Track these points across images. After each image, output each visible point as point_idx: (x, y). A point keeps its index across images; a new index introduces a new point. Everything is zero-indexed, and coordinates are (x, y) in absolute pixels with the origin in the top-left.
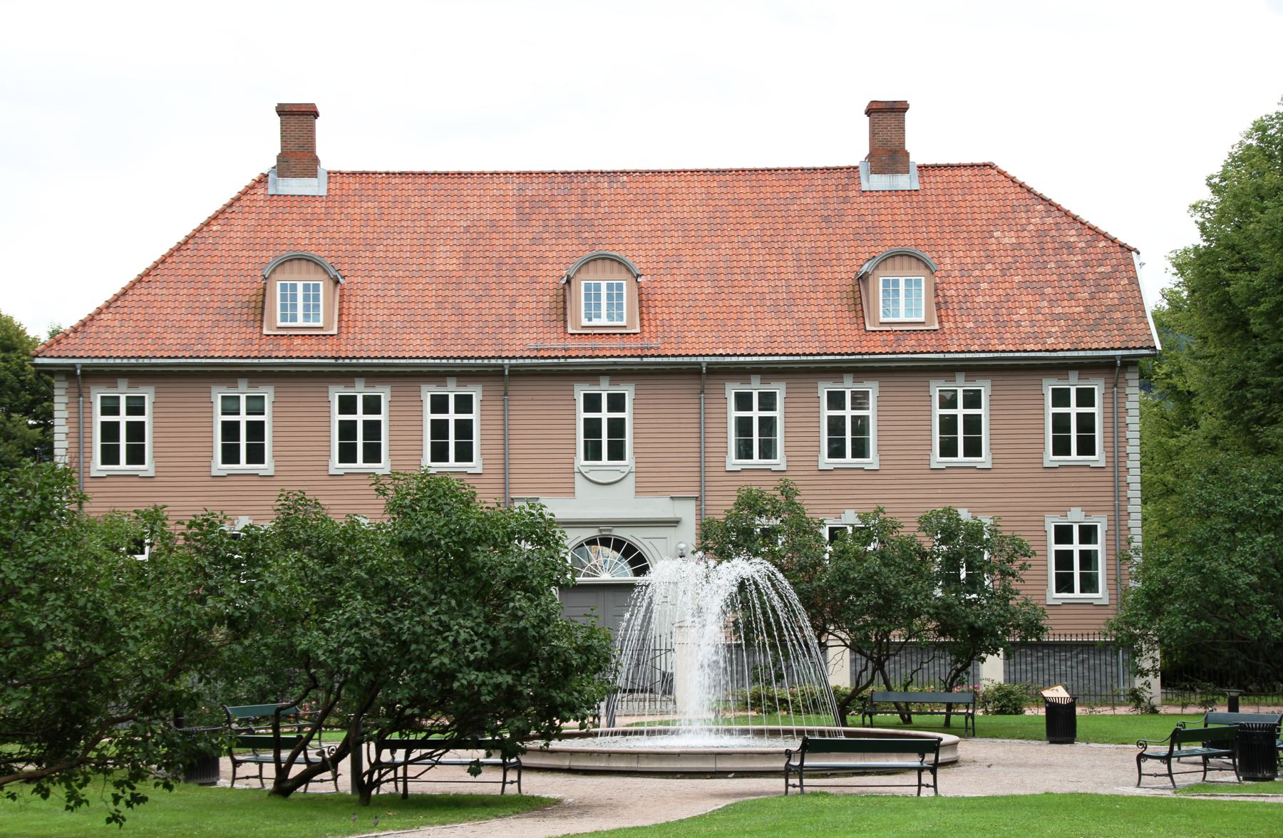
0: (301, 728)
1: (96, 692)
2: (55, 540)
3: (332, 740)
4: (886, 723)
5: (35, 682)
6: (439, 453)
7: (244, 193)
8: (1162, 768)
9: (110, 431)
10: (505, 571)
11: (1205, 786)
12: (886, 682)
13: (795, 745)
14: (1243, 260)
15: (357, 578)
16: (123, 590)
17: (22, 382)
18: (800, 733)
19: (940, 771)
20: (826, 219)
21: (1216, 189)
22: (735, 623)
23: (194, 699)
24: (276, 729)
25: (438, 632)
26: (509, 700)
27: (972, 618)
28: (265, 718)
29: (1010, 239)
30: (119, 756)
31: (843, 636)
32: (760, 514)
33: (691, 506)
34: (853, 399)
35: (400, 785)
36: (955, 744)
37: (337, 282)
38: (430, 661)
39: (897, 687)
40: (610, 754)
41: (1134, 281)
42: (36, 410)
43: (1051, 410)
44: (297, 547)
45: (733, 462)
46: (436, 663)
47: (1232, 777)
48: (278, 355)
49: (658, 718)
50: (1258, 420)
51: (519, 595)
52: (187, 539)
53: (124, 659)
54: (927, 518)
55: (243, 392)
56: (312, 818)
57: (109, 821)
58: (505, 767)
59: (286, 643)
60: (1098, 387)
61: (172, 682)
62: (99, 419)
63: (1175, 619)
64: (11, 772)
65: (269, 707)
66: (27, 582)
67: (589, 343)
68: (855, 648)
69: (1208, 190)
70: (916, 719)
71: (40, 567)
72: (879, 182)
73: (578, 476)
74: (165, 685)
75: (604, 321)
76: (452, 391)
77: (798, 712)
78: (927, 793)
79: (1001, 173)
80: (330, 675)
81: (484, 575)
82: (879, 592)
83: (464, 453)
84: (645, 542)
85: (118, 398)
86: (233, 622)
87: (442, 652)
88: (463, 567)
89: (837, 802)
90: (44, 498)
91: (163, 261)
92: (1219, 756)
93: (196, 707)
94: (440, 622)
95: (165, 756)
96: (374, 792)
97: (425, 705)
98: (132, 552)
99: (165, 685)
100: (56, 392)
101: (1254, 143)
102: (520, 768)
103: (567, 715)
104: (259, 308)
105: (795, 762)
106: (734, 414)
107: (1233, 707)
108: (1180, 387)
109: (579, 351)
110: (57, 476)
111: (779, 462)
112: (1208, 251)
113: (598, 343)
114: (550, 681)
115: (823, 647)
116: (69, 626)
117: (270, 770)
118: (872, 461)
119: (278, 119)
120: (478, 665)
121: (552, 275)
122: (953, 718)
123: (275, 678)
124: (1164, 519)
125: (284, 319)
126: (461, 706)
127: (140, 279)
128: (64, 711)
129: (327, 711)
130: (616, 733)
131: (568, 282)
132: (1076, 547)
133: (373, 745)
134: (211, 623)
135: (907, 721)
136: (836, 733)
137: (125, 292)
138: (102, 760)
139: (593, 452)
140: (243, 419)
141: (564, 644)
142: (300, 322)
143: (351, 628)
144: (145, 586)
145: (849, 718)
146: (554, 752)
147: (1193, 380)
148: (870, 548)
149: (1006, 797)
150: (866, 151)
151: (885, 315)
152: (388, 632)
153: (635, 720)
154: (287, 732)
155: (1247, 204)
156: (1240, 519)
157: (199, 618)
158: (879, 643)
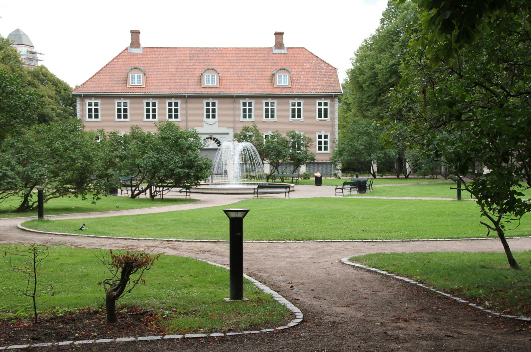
0: (137, 182)
1: (88, 173)
2: (77, 136)
3: (145, 185)
4: (278, 182)
5: (73, 170)
6: (170, 117)
7: (122, 52)
8: (341, 191)
9: (90, 110)
10: (187, 145)
11: (350, 195)
12: (278, 172)
13: (256, 187)
14: (362, 72)
15: (151, 147)
16: (94, 149)
17: (69, 98)
18: (257, 184)
19: (290, 193)
20: (264, 60)
21: (356, 55)
22: (242, 158)
23: (111, 175)
24: (131, 182)
25: (171, 160)
26: (188, 176)
27: (298, 157)
28: (129, 180)
29: (308, 66)
30: (94, 188)
31: (268, 161)
32: (248, 132)
33: (232, 130)
34: (271, 104)
35: (161, 196)
36: (294, 186)
37: (145, 74)
38: (169, 166)
39: (281, 173)
40: (212, 189)
41: (337, 76)
42: (73, 105)
43: (291, 107)
44: (136, 139)
45: (242, 119)
46: (170, 167)
47: (356, 193)
48: (130, 92)
49: (224, 181)
50: (365, 110)
51: (190, 151)
52: (110, 137)
53: (94, 165)
54: (288, 133)
55: (122, 101)
56: (140, 204)
57: (92, 203)
58: (186, 192)
59: (133, 162)
60: (328, 101)
61: (106, 171)
62: (88, 107)
63: (345, 157)
64: (69, 191)
65: (130, 177)
66: (71, 146)
67: (206, 90)
68: (271, 164)
69: (354, 55)
70: (285, 181)
71: (74, 143)
72: (277, 51)
73: (204, 122)
74: (104, 172)
75: (210, 84)
76: (173, 101)
77: (257, 179)
78: (287, 198)
79: (306, 50)
80: (144, 170)
81: (182, 146)
82: (277, 151)
83: (176, 117)
84: (221, 139)
85: (121, 103)
86: (121, 158)
87: (171, 164)
88: (176, 144)
89: (266, 200)
90: (75, 126)
91: (102, 69)
92: (354, 188)
93: (112, 177)
94: (171, 157)
95: (105, 189)
96: (155, 198)
97: (168, 177)
98: (96, 140)
99: (104, 172)
100: (77, 101)
101: (364, 44)
102: (190, 192)
103: (201, 179)
104: (126, 81)
105: (256, 191)
106: (242, 107)
107: (357, 177)
108: (347, 102)
109: (204, 92)
110: (78, 121)
111: (253, 119)
112: (354, 70)
113: (209, 90)
114: (197, 171)
115: (263, 164)
116: (81, 157)
117: (130, 192)
118: (275, 119)
119: (131, 34)
120: (180, 167)
121: (198, 73)
122: (294, 180)
123: (131, 170)
124: (343, 133)
125: (132, 83)
126: (176, 177)
127: (97, 73)
128: (81, 177)
129: (144, 178)
130: (213, 184)
131: (202, 75)
132: (323, 140)
133: (155, 187)
134: (115, 157)
135: (283, 181)
136: (266, 184)
137: (93, 76)
138: (90, 189)
139: (208, 116)
140: (122, 108)
141: (201, 162)
142: (136, 84)
143: (149, 159)
144: (99, 148)
145: (269, 180)
146: (198, 189)
147: (350, 100)
148: (275, 140)
149: (305, 198)
150: (274, 44)
151: (279, 84)
152: (158, 160)
153: (218, 181)
154: (134, 183)
155: (362, 59)
156: (360, 133)
157: (112, 156)
158: (276, 163)
